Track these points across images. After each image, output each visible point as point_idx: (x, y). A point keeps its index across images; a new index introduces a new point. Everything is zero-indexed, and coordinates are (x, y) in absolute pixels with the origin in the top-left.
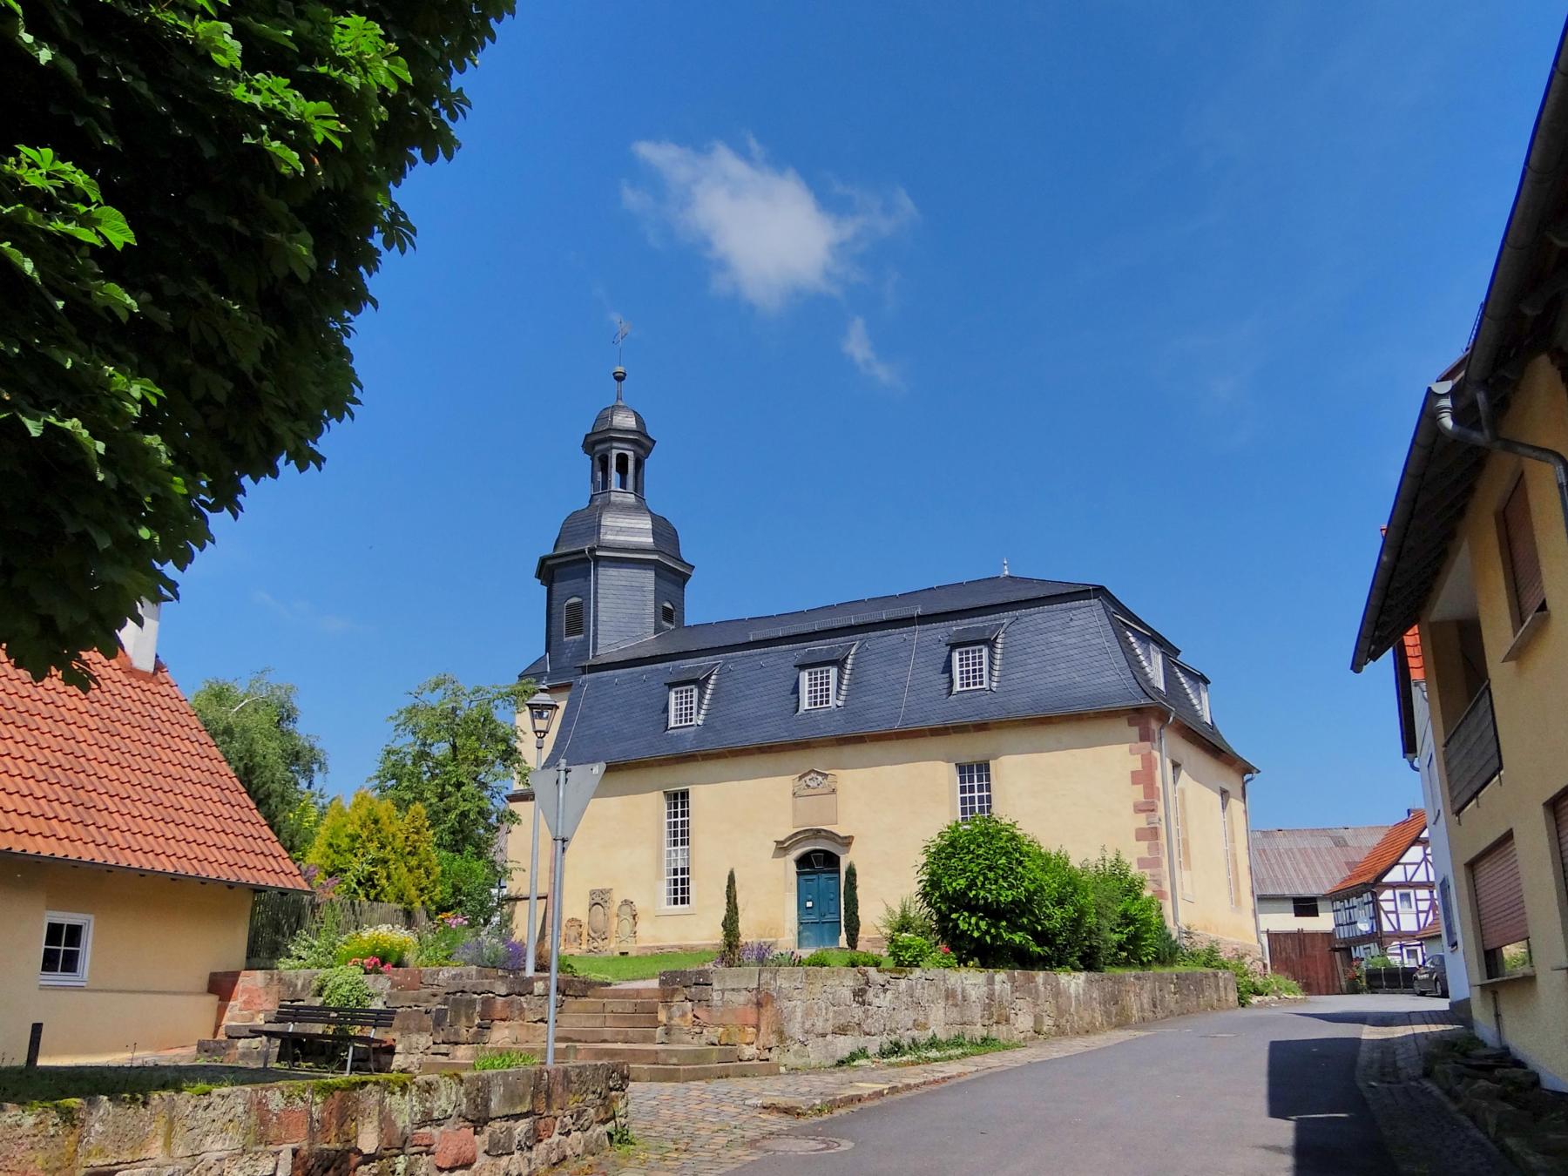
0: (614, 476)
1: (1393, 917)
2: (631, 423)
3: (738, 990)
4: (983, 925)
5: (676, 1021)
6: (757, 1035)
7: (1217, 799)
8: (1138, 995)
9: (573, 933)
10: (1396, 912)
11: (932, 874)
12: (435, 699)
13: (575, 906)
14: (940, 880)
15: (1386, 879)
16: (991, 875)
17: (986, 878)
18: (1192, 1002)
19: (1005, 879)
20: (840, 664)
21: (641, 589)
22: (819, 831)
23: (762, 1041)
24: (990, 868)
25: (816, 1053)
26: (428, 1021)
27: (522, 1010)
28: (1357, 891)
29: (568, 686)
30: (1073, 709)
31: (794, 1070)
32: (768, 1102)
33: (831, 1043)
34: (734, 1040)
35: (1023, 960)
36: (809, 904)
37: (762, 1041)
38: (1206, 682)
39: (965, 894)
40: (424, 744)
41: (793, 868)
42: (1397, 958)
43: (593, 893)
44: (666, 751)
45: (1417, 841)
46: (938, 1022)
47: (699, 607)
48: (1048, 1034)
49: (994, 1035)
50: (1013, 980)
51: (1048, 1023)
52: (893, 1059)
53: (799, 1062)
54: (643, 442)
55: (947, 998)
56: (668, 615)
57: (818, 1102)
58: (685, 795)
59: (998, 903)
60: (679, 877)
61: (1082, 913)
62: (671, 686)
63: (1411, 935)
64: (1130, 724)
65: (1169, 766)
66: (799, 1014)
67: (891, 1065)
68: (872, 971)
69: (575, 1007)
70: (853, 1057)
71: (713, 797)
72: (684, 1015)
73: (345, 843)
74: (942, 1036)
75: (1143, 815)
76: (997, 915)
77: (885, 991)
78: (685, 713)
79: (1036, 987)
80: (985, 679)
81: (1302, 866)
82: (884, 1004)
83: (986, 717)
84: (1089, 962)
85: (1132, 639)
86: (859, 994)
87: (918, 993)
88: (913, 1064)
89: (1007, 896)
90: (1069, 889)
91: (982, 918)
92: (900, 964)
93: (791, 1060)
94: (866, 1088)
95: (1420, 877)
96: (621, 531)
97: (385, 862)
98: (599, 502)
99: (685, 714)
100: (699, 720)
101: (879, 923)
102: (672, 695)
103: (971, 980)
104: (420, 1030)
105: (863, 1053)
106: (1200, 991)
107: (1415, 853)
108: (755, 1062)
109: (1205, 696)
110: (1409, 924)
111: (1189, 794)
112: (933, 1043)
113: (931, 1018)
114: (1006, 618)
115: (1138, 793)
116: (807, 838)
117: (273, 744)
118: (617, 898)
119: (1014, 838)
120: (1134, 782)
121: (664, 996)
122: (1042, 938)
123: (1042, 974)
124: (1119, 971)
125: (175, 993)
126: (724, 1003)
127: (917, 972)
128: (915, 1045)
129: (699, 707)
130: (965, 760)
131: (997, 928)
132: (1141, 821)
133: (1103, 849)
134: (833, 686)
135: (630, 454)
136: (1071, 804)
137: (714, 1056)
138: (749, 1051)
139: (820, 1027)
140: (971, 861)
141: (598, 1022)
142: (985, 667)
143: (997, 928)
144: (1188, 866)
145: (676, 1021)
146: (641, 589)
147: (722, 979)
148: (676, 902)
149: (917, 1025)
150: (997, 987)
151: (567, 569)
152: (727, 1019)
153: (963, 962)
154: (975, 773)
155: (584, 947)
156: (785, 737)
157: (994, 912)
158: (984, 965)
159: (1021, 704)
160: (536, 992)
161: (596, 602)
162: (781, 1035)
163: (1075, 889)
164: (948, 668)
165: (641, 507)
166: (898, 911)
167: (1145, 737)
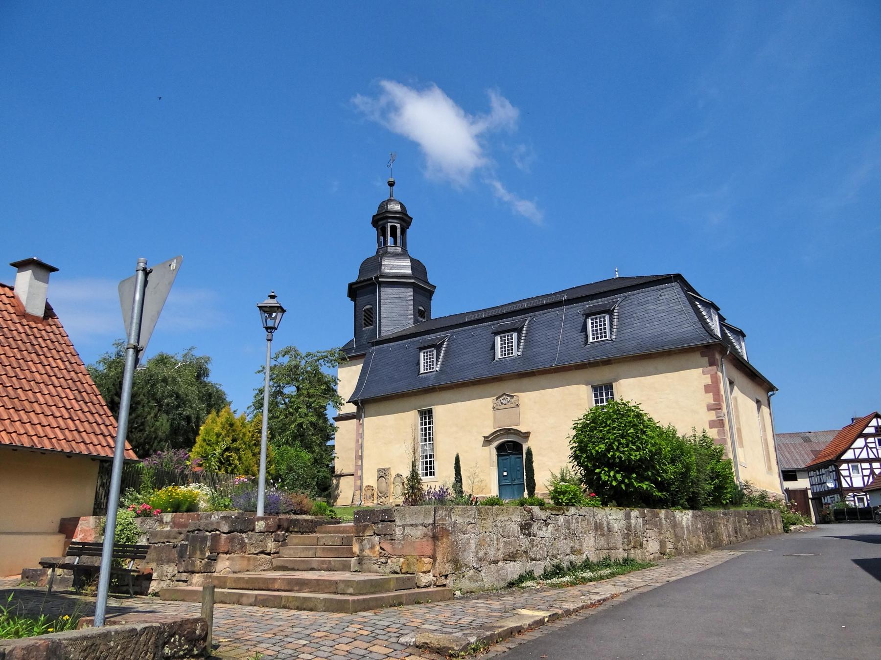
0: (390, 240)
1: (848, 479)
2: (398, 208)
3: (416, 525)
4: (619, 477)
5: (367, 552)
6: (434, 564)
7: (755, 405)
8: (726, 525)
9: (369, 494)
10: (850, 476)
11: (581, 442)
12: (285, 361)
13: (370, 479)
14: (586, 446)
15: (843, 458)
16: (623, 441)
17: (620, 443)
18: (758, 530)
19: (634, 444)
20: (519, 331)
21: (405, 299)
22: (509, 429)
23: (439, 568)
24: (622, 436)
25: (488, 577)
26: (175, 554)
27: (243, 545)
28: (825, 465)
29: (363, 355)
30: (665, 348)
31: (468, 595)
32: (421, 640)
33: (502, 568)
34: (414, 568)
35: (646, 501)
36: (505, 474)
37: (439, 568)
38: (744, 336)
39: (605, 455)
40: (279, 386)
41: (494, 452)
42: (852, 502)
43: (379, 470)
44: (419, 386)
45: (861, 435)
46: (590, 548)
47: (439, 308)
48: (670, 555)
49: (632, 556)
50: (643, 515)
51: (670, 546)
52: (555, 580)
53: (474, 586)
54: (405, 220)
55: (596, 530)
56: (421, 314)
57: (473, 640)
58: (430, 412)
59: (630, 460)
60: (428, 460)
61: (688, 468)
62: (421, 349)
63: (859, 489)
64: (702, 356)
65: (728, 382)
66: (473, 545)
67: (554, 586)
68: (536, 509)
69: (295, 541)
70: (522, 579)
71: (448, 414)
72: (372, 547)
73: (213, 439)
74: (593, 559)
75: (714, 412)
76: (630, 469)
77: (547, 525)
78: (428, 364)
79: (660, 520)
80: (608, 334)
81: (786, 453)
82: (546, 535)
83: (609, 356)
84: (693, 504)
85: (699, 306)
86: (526, 528)
87: (574, 526)
88: (572, 584)
89: (636, 456)
90: (678, 452)
91: (618, 472)
92: (558, 503)
93: (466, 584)
94: (531, 615)
95: (864, 455)
96: (393, 267)
97: (237, 450)
98: (382, 252)
99: (429, 365)
100: (437, 368)
101: (547, 484)
102: (422, 354)
103: (613, 517)
104: (169, 561)
105: (529, 576)
106: (762, 523)
107: (860, 442)
108: (432, 589)
109: (743, 344)
110: (858, 483)
111: (739, 401)
112: (587, 565)
113: (585, 545)
114: (619, 297)
115: (709, 398)
116: (502, 434)
117: (193, 389)
118: (393, 473)
119: (639, 416)
120: (707, 391)
121: (358, 532)
122: (662, 486)
123: (663, 511)
124: (712, 510)
125: (36, 533)
126: (405, 537)
127: (573, 510)
128: (573, 567)
129: (437, 361)
130: (598, 383)
131: (629, 479)
132: (712, 416)
133: (694, 429)
134: (515, 344)
135: (398, 225)
136: (673, 401)
137: (392, 585)
138: (425, 579)
139: (492, 553)
140: (608, 432)
141: (311, 553)
142: (608, 326)
143: (629, 479)
144: (741, 445)
145: (367, 552)
146: (405, 299)
147: (403, 517)
148: (427, 475)
149: (573, 551)
150: (633, 521)
151: (364, 289)
152: (407, 551)
153: (605, 504)
154: (603, 390)
155: (375, 502)
156: (487, 375)
157: (626, 467)
158: (620, 505)
159: (631, 347)
160: (257, 528)
161: (380, 307)
162: (457, 564)
163: (682, 453)
164: (584, 329)
165: (404, 254)
166: (559, 476)
167: (712, 363)
